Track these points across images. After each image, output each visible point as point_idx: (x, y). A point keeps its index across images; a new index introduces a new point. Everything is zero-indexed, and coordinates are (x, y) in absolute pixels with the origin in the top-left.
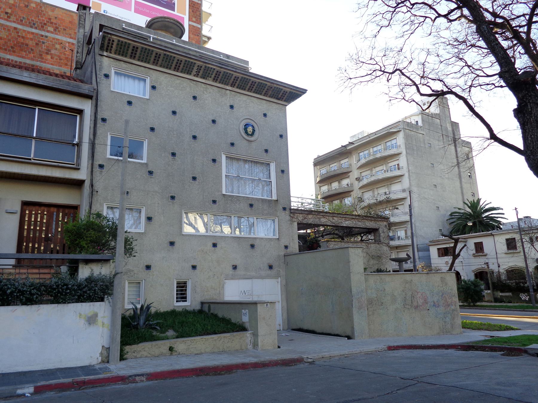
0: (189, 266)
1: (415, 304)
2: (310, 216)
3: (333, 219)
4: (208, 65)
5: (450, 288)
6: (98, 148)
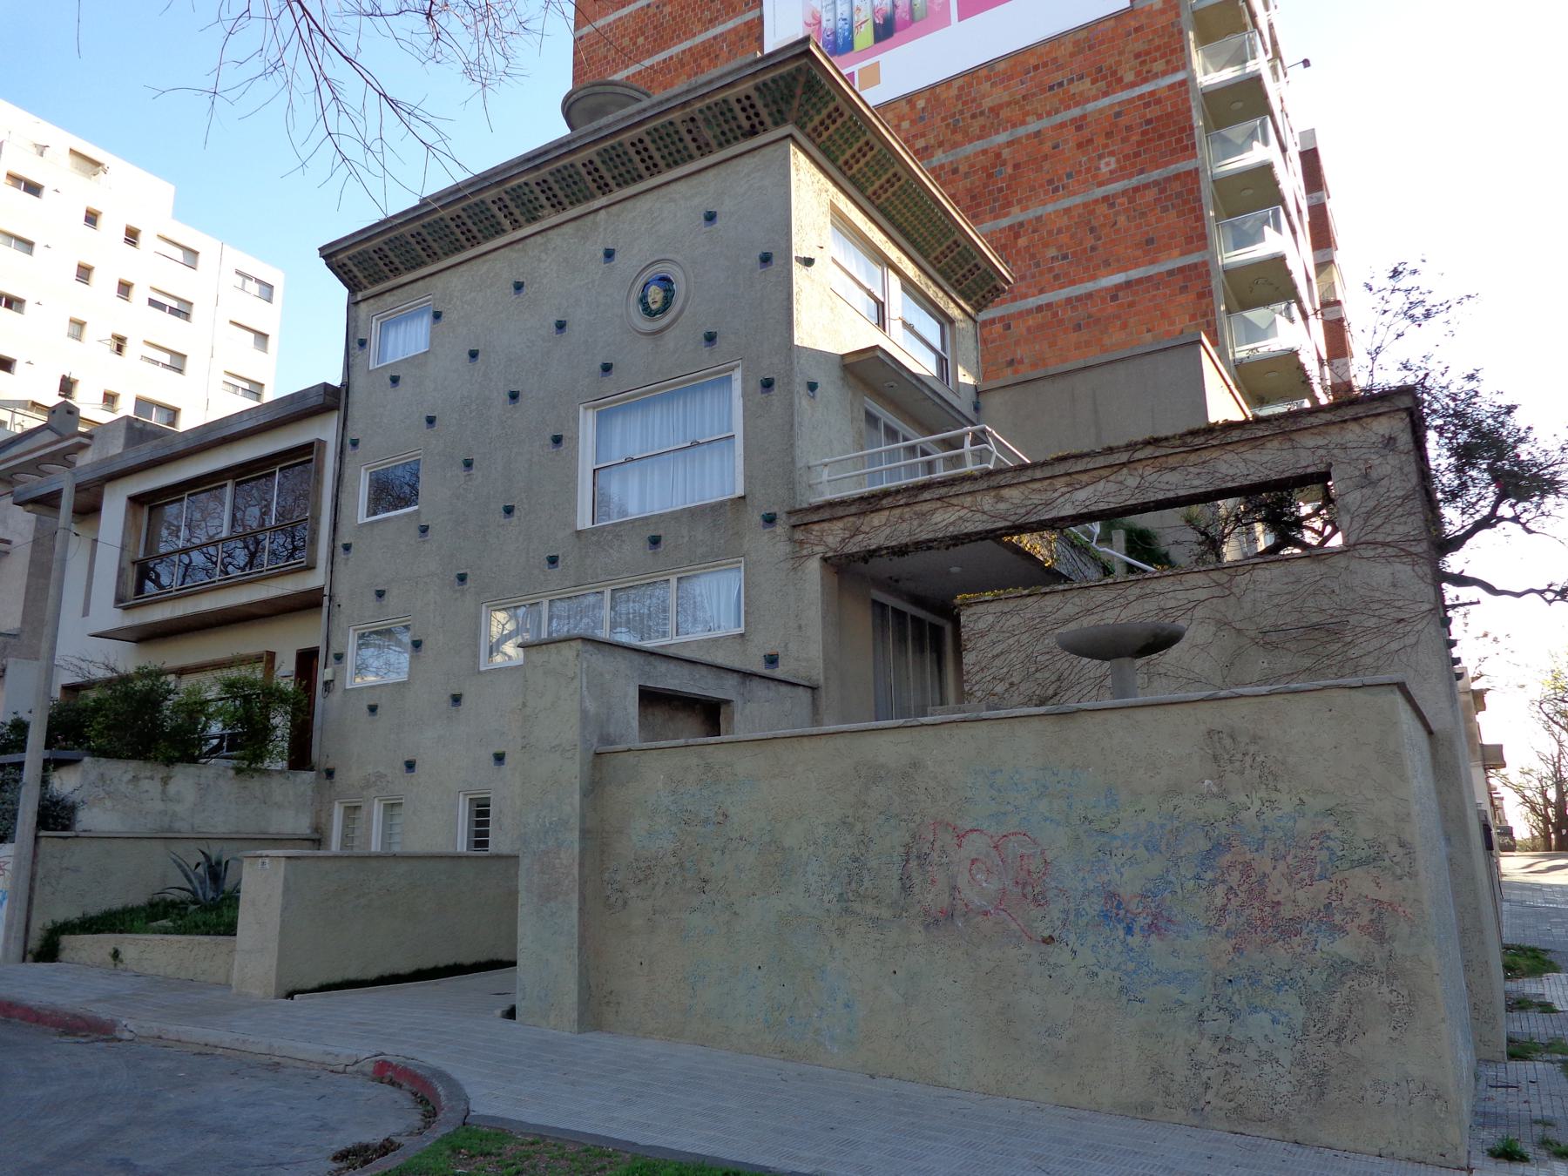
0: (487, 756)
1: (933, 898)
2: (877, 519)
3: (1000, 499)
4: (508, 186)
6: (345, 511)
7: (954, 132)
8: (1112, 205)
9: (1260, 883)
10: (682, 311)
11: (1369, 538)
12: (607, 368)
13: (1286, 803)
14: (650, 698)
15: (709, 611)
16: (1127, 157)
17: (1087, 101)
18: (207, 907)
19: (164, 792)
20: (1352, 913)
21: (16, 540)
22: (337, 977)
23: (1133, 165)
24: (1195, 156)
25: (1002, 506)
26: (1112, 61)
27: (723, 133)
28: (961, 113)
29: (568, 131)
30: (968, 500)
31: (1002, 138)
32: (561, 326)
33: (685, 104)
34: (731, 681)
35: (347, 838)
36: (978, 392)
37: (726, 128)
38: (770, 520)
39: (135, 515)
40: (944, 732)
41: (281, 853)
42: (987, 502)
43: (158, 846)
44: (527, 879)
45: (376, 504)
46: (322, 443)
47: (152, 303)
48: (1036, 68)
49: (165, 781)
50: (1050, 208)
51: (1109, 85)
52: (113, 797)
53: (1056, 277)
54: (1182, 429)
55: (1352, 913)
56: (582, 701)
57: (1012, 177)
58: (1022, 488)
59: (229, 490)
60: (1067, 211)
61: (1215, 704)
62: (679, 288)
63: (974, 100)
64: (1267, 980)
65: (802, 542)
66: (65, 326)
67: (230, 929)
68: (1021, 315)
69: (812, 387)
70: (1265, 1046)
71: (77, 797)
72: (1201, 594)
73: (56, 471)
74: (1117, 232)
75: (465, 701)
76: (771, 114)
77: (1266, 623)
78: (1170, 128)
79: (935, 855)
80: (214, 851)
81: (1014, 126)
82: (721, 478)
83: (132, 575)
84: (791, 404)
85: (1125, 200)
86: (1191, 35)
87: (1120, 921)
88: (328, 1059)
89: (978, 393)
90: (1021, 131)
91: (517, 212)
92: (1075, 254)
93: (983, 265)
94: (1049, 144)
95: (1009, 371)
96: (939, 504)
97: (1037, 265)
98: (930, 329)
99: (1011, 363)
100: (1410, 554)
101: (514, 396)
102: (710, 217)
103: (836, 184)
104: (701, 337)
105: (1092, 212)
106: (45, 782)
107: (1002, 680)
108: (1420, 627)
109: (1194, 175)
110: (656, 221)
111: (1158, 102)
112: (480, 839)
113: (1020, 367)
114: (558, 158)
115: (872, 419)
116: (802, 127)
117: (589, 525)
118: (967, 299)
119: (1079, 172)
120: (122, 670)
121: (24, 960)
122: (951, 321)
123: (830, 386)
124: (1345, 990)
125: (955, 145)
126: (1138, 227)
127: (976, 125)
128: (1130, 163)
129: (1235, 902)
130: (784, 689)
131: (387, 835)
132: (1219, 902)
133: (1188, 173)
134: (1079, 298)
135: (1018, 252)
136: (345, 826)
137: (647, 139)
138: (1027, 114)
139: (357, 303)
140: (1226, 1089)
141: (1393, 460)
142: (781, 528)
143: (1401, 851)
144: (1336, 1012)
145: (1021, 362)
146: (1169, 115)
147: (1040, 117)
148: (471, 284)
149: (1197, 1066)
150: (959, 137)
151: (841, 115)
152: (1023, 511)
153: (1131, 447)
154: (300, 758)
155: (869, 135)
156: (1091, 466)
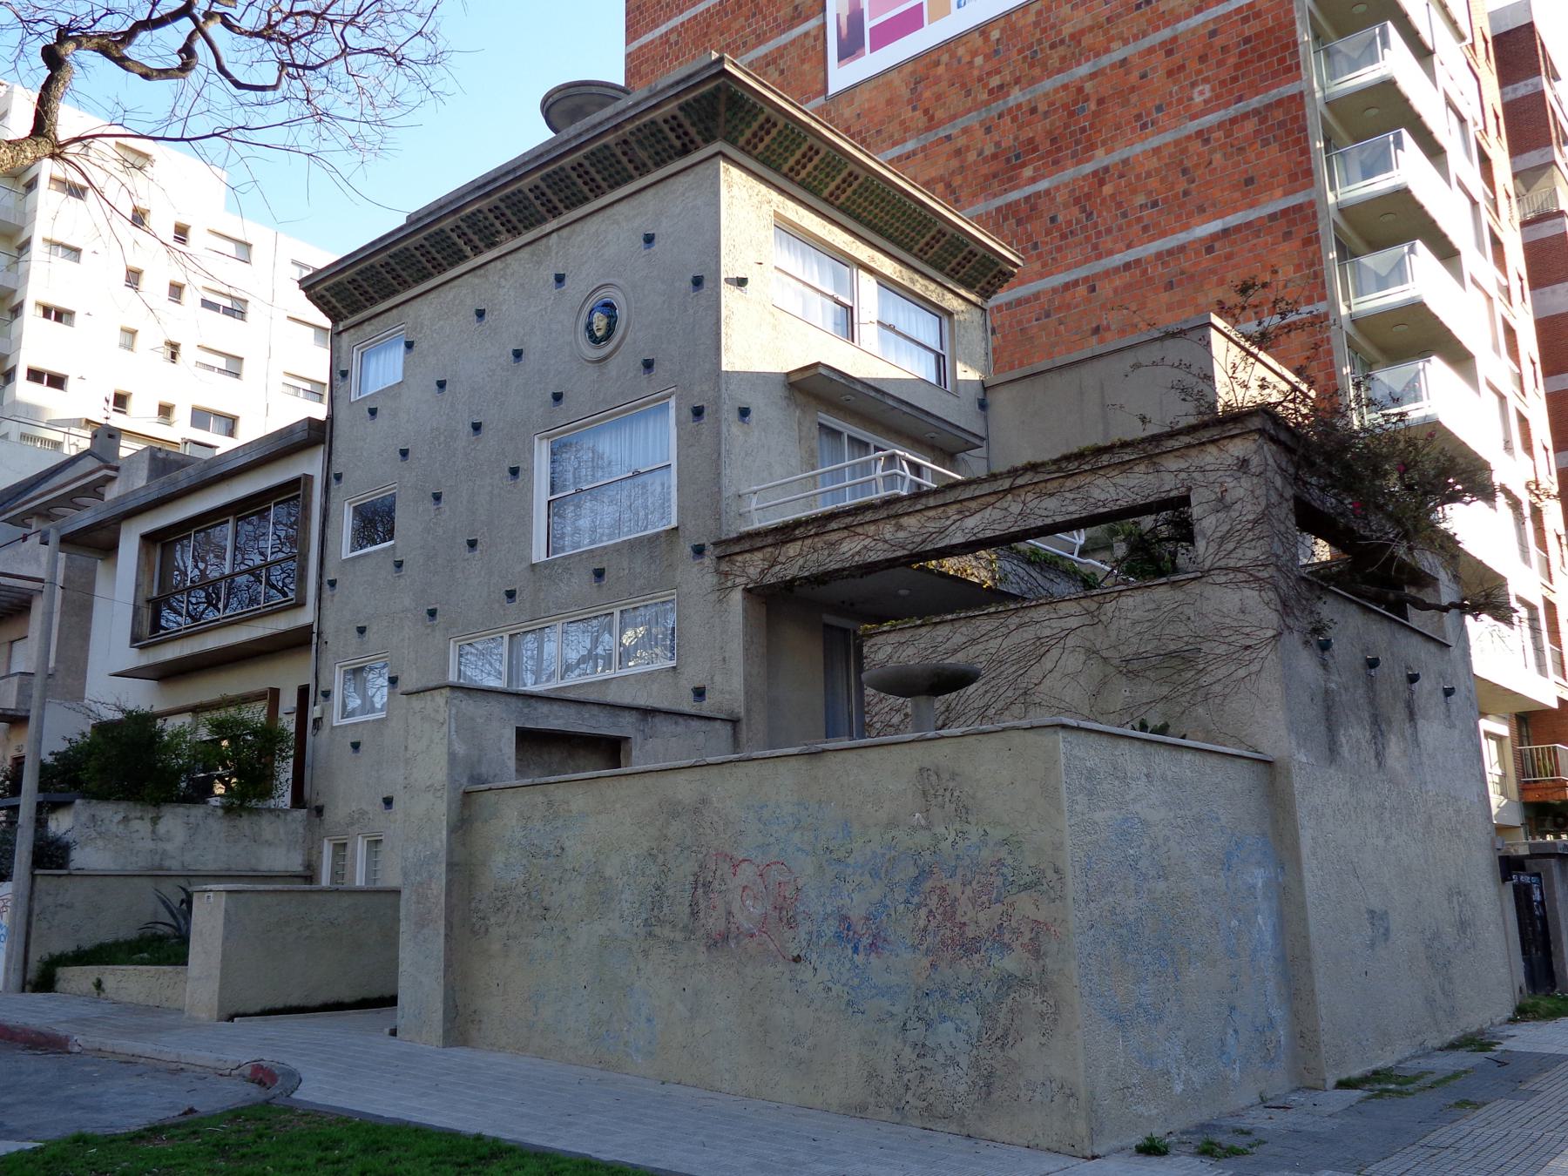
1: (713, 922)
2: (792, 549)
3: (900, 527)
5: (997, 834)
6: (330, 547)
7: (1032, 66)
9: (952, 905)
10: (623, 338)
11: (1222, 563)
12: (558, 397)
13: (974, 834)
14: (528, 739)
16: (1223, 83)
17: (1178, 20)
19: (153, 832)
20: (1017, 932)
22: (280, 1004)
23: (1230, 92)
24: (1299, 77)
25: (901, 534)
27: (657, 153)
28: (1040, 42)
29: (551, 134)
30: (872, 529)
31: (1084, 70)
32: (518, 354)
33: (617, 127)
35: (336, 874)
36: (985, 387)
37: (659, 147)
38: (699, 551)
39: (148, 553)
40: (726, 769)
41: (221, 887)
42: (888, 530)
43: (148, 884)
44: (407, 906)
47: (206, 304)
49: (155, 821)
50: (1138, 148)
52: (102, 837)
53: (1145, 229)
55: (1017, 932)
56: (450, 743)
57: (1096, 114)
58: (919, 516)
59: (230, 525)
60: (1157, 150)
61: (925, 744)
62: (622, 313)
63: (1053, 27)
64: (954, 993)
65: (726, 574)
66: (117, 337)
67: (186, 964)
68: (1107, 274)
69: (744, 412)
70: (950, 1052)
71: (69, 837)
72: (1073, 623)
73: (90, 504)
74: (1213, 171)
76: (699, 133)
77: (1128, 651)
79: (716, 883)
81: (1097, 55)
82: (662, 508)
83: (146, 615)
84: (719, 433)
85: (1221, 133)
87: (849, 941)
88: (218, 1065)
89: (985, 389)
90: (1105, 60)
91: (475, 238)
92: (1165, 200)
93: (981, 251)
94: (1136, 74)
95: (1095, 339)
96: (846, 533)
97: (1125, 215)
98: (925, 327)
99: (1096, 330)
100: (1257, 579)
101: (477, 427)
102: (649, 239)
103: (781, 191)
104: (639, 364)
105: (1184, 151)
106: (41, 823)
107: (898, 711)
108: (1264, 654)
109: (1298, 100)
111: (1257, 15)
113: (1108, 335)
114: (505, 185)
115: (835, 434)
116: (733, 143)
117: (544, 558)
118: (969, 287)
119: (1170, 104)
120: (131, 707)
121: (23, 990)
122: (950, 314)
123: (767, 409)
124: (1009, 1001)
125: (1033, 81)
126: (1237, 165)
127: (1054, 59)
128: (1229, 90)
129: (934, 923)
130: (695, 724)
131: (371, 871)
132: (922, 923)
133: (1292, 98)
134: (1170, 252)
135: (1104, 201)
137: (586, 163)
138: (1111, 39)
139: (339, 333)
140: (921, 1090)
141: (1246, 482)
142: (708, 560)
143: (1055, 877)
144: (1002, 1021)
145: (1108, 328)
146: (1270, 31)
147: (1126, 42)
148: (437, 310)
149: (901, 1070)
150: (1037, 71)
151: (775, 125)
152: (918, 539)
153: (1014, 472)
155: (811, 140)
156: (977, 493)
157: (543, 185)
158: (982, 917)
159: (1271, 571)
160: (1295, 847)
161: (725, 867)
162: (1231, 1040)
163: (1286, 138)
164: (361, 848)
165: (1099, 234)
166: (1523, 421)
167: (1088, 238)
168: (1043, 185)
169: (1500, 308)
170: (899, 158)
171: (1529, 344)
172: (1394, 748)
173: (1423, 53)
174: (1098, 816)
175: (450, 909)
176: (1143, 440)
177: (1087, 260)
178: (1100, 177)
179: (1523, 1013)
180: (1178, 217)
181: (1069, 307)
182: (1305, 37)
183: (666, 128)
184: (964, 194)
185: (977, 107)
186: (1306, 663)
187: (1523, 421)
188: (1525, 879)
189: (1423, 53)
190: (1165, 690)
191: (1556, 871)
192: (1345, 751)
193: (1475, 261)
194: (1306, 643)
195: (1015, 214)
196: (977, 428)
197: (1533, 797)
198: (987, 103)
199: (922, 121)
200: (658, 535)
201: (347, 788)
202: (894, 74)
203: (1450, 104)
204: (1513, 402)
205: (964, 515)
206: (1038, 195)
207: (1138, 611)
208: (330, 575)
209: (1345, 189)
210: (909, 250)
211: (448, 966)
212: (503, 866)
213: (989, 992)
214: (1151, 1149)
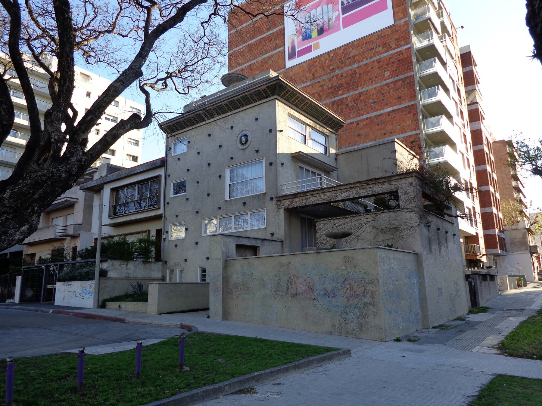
1: (293, 291)
2: (297, 199)
3: (325, 195)
6: (167, 194)
8: (388, 86)
13: (358, 271)
15: (253, 225)
16: (393, 71)
18: (139, 295)
20: (368, 293)
21: (79, 198)
22: (170, 311)
23: (395, 74)
25: (325, 197)
26: (388, 41)
31: (356, 66)
32: (220, 146)
33: (249, 91)
34: (259, 241)
35: (171, 279)
36: (336, 154)
38: (272, 199)
42: (322, 196)
43: (126, 281)
45: (177, 192)
46: (161, 176)
48: (366, 43)
49: (127, 265)
50: (370, 87)
51: (388, 49)
52: (116, 269)
53: (372, 109)
54: (365, 180)
55: (368, 293)
57: (359, 78)
59: (136, 188)
60: (375, 88)
63: (348, 54)
67: (146, 300)
68: (362, 120)
71: (108, 269)
72: (369, 220)
75: (199, 244)
77: (383, 227)
78: (404, 62)
80: (140, 282)
81: (359, 62)
82: (261, 187)
83: (112, 209)
86: (412, 32)
90: (362, 63)
92: (377, 101)
93: (336, 120)
94: (370, 67)
97: (366, 105)
98: (322, 139)
99: (359, 135)
101: (209, 165)
102: (257, 119)
103: (290, 107)
109: (413, 77)
110: (243, 119)
111: (402, 54)
112: (203, 278)
115: (302, 168)
116: (279, 96)
123: (288, 163)
125: (342, 68)
128: (394, 73)
130: (273, 242)
132: (345, 291)
134: (379, 115)
136: (170, 276)
138: (363, 58)
141: (412, 188)
146: (405, 58)
147: (367, 59)
148: (197, 133)
149: (340, 324)
150: (343, 65)
153: (354, 183)
154: (158, 258)
157: (228, 104)
158: (359, 290)
159: (418, 209)
160: (423, 274)
161: (296, 278)
162: (410, 317)
163: (409, 87)
164: (178, 272)
165: (359, 110)
166: (468, 159)
167: (357, 111)
168: (344, 96)
169: (462, 130)
170: (305, 87)
171: (469, 139)
172: (443, 249)
173: (444, 64)
174: (385, 267)
175: (223, 288)
176: (387, 177)
177: (356, 116)
178: (360, 94)
179: (470, 312)
180: (381, 106)
181: (351, 129)
182: (414, 60)
183: (262, 92)
184: (323, 97)
185: (327, 74)
186: (425, 230)
187: (468, 159)
188: (470, 280)
189: (444, 64)
190: (392, 236)
191: (477, 278)
192: (433, 251)
193: (457, 119)
194: (425, 226)
195: (337, 103)
196: (334, 165)
197: (469, 258)
198: (329, 73)
199: (312, 77)
200: (260, 194)
201: (173, 257)
202: (304, 64)
203: (450, 77)
204: (465, 155)
205: (342, 193)
206: (343, 98)
207: (385, 217)
208: (167, 201)
209: (425, 100)
210: (319, 120)
211: (223, 301)
212: (236, 277)
213: (361, 306)
214: (398, 340)
